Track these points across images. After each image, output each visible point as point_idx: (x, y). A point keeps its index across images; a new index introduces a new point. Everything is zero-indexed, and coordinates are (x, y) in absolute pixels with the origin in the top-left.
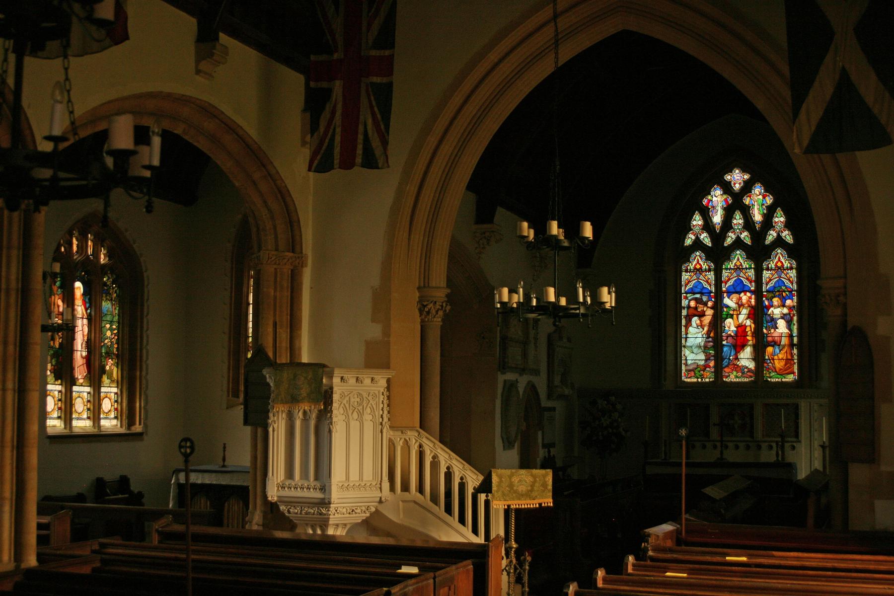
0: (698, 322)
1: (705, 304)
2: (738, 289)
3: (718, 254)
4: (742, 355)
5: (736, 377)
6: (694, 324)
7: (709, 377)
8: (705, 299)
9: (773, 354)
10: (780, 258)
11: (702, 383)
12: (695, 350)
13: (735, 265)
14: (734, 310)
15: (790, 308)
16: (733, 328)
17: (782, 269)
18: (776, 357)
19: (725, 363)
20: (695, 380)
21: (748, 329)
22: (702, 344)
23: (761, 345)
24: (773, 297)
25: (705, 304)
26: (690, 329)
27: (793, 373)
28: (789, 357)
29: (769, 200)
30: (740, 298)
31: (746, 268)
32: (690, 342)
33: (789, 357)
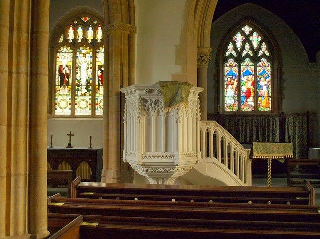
3: (240, 60)
4: (249, 100)
7: (236, 109)
12: (230, 98)
17: (265, 67)
19: (242, 103)
20: (230, 110)
21: (251, 90)
25: (234, 80)
32: (228, 95)
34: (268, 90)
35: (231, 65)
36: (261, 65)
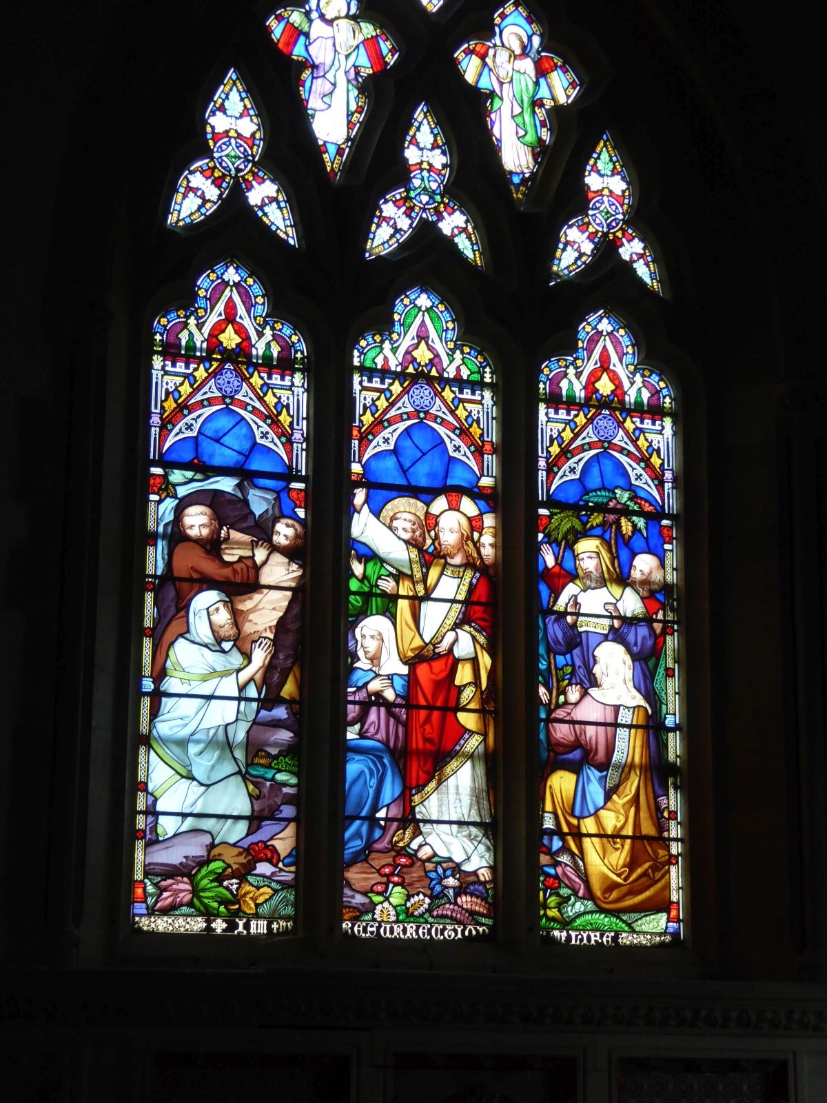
0: (223, 617)
1: (262, 531)
2: (422, 475)
3: (331, 294)
4: (431, 805)
5: (408, 915)
6: (200, 627)
7: (265, 906)
8: (259, 503)
9: (576, 808)
10: (606, 357)
11: (229, 941)
12: (202, 766)
13: (409, 358)
14: (398, 576)
15: (653, 593)
16: (393, 665)
17: (614, 403)
18: (589, 825)
19: (354, 836)
20: (198, 925)
21: (464, 675)
22: (240, 734)
23: (521, 764)
24: (585, 534)
25: (262, 531)
26: (181, 647)
27: (661, 905)
28: (648, 829)
29: (561, 88)
30: (430, 523)
31: (458, 382)
32: (176, 719)
33: (648, 829)
34: (651, 695)
35: (230, 339)
36: (573, 385)
